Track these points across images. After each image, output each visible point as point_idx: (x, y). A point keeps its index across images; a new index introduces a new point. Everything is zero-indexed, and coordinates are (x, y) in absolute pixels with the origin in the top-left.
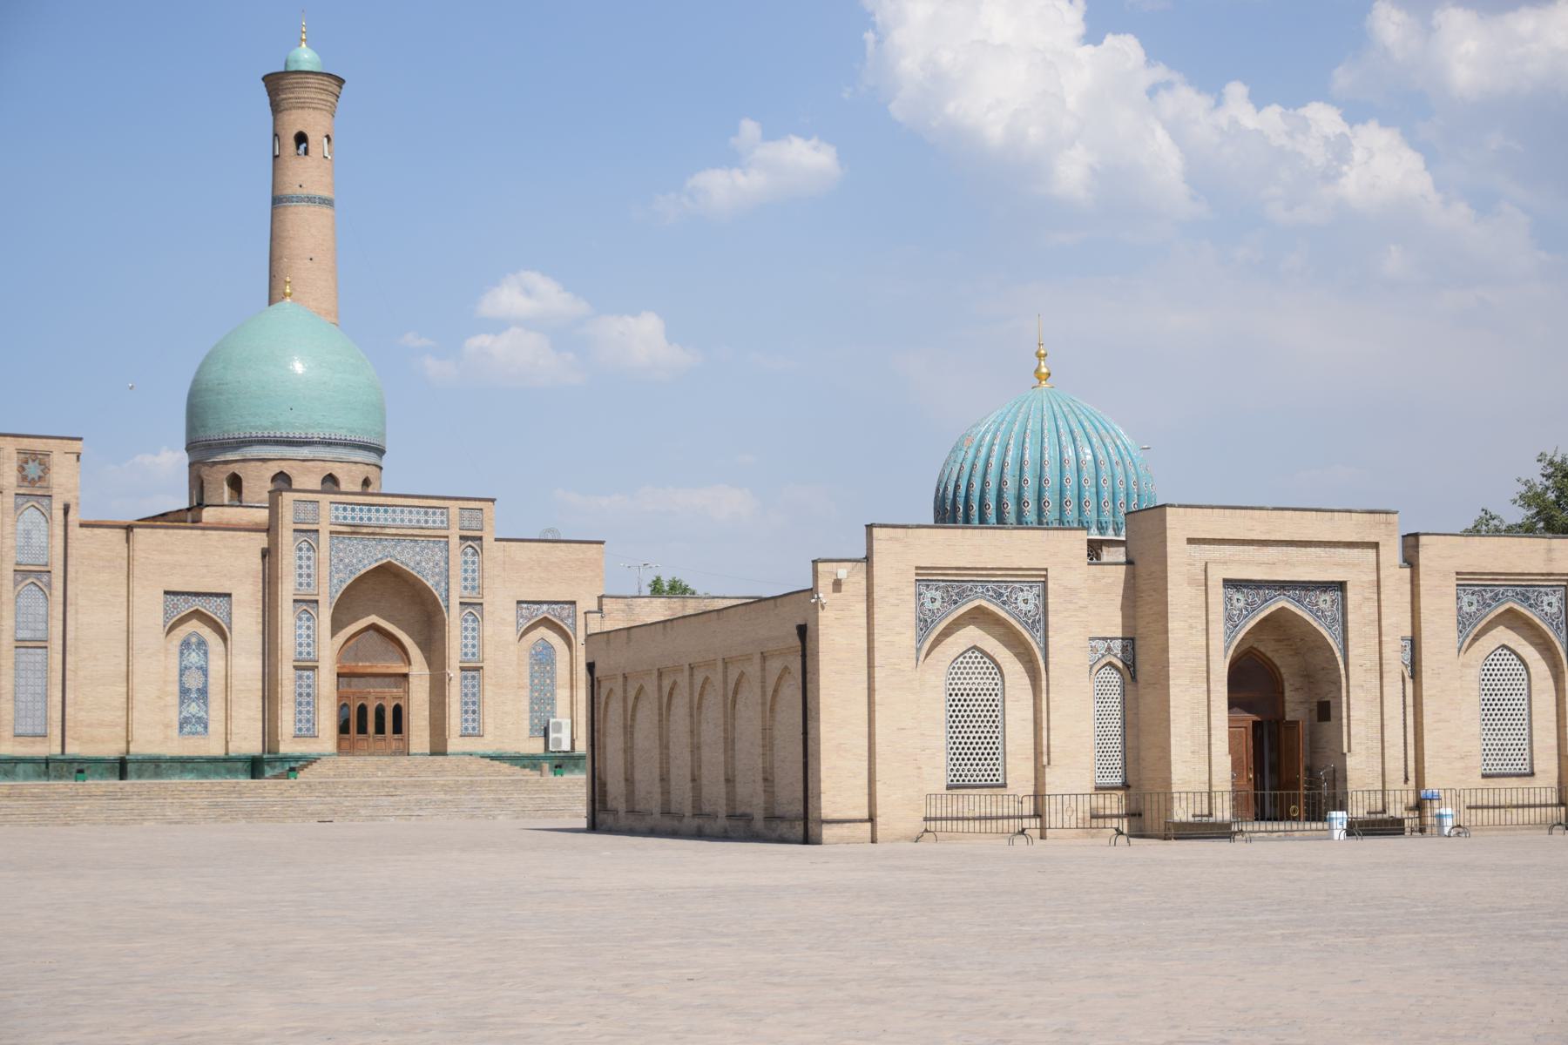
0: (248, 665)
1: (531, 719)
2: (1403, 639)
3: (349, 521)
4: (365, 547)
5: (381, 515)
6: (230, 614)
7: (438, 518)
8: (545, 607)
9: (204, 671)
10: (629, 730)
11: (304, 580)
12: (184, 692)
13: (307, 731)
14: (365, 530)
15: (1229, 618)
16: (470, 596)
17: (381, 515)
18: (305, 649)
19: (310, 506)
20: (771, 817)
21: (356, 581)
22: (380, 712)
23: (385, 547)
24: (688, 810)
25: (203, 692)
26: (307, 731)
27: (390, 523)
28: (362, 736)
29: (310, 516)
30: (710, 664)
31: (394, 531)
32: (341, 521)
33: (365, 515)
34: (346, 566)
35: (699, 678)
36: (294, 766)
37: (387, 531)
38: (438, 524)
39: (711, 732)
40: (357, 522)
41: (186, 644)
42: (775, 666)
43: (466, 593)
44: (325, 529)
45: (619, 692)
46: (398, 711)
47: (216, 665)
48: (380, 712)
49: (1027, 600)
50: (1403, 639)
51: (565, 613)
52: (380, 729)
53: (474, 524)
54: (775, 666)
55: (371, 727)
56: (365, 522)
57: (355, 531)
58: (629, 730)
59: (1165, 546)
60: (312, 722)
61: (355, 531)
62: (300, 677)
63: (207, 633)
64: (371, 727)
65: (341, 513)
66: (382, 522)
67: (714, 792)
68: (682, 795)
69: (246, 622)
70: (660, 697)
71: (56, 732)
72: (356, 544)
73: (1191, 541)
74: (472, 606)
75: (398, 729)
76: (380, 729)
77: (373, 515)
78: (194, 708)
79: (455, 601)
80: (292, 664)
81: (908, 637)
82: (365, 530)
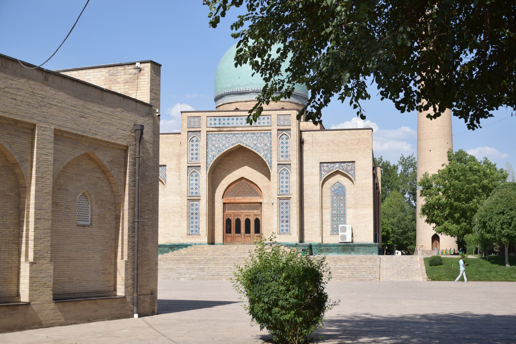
1: (332, 225)
3: (217, 125)
4: (226, 138)
5: (235, 121)
6: (165, 175)
7: (266, 121)
8: (337, 165)
11: (194, 156)
14: (225, 129)
16: (283, 160)
17: (235, 121)
18: (194, 191)
19: (197, 119)
21: (254, 153)
22: (248, 221)
23: (237, 138)
27: (239, 125)
28: (238, 235)
29: (197, 124)
31: (241, 129)
32: (213, 125)
33: (226, 122)
34: (216, 148)
37: (238, 129)
38: (266, 124)
40: (221, 125)
43: (282, 159)
44: (204, 130)
46: (257, 222)
48: (248, 221)
51: (349, 168)
52: (248, 231)
53: (286, 123)
55: (243, 230)
56: (226, 125)
57: (42, 135)
59: (158, 223)
61: (220, 130)
62: (192, 205)
63: (246, 172)
64: (243, 230)
65: (213, 122)
66: (235, 125)
70: (83, 300)
72: (221, 137)
73: (180, 133)
75: (258, 230)
76: (248, 231)
77: (230, 121)
79: (275, 163)
80: (201, 198)
82: (225, 129)
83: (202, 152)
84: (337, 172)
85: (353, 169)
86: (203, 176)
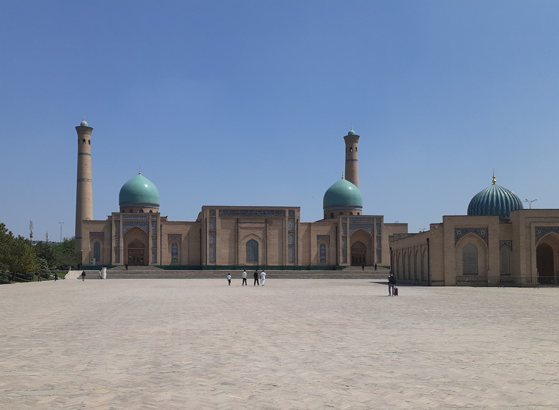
0: (333, 249)
2: (19, 236)
9: (325, 250)
10: (398, 262)
12: (321, 254)
13: (345, 261)
15: (537, 235)
16: (378, 235)
20: (423, 280)
24: (420, 279)
25: (325, 254)
26: (345, 261)
30: (411, 247)
35: (398, 252)
36: (341, 268)
39: (401, 264)
41: (321, 245)
42: (423, 248)
45: (401, 253)
46: (364, 257)
47: (327, 249)
48: (360, 257)
49: (483, 232)
50: (19, 236)
54: (423, 248)
58: (398, 262)
60: (119, 259)
67: (413, 277)
68: (413, 277)
69: (332, 241)
71: (296, 261)
74: (379, 239)
78: (175, 256)
81: (453, 241)
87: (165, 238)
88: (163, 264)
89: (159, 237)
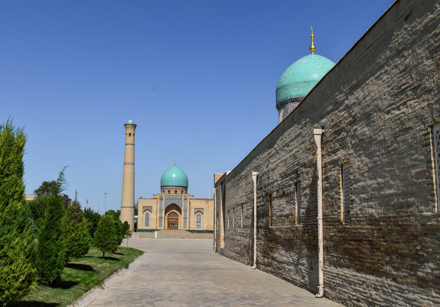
83: (164, 205)
84: (199, 211)
85: (152, 209)
86: (164, 212)
87: (193, 211)
88: (191, 229)
89: (188, 210)
